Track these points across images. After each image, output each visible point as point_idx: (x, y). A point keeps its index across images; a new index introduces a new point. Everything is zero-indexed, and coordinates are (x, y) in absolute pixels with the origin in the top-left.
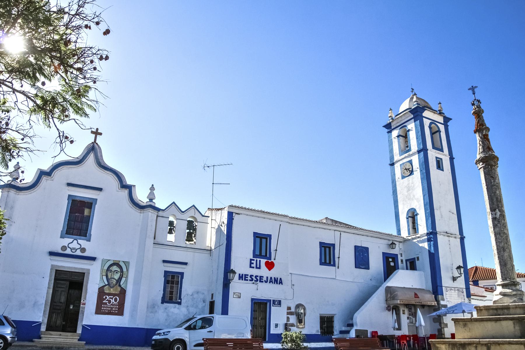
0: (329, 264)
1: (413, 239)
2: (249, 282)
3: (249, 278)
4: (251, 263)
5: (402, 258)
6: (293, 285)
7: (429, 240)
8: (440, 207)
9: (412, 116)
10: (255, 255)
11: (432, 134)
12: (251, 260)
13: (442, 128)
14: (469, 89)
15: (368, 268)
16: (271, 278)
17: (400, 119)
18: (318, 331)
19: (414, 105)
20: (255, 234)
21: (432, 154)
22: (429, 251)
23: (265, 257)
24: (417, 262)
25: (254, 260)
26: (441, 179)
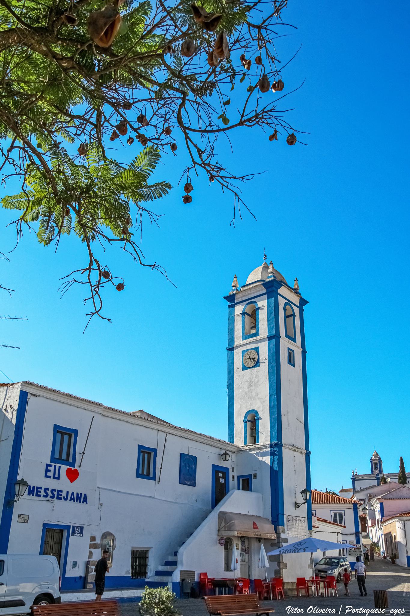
0: (147, 476)
1: (251, 450)
2: (42, 498)
3: (43, 493)
4: (47, 471)
6: (101, 505)
7: (272, 454)
8: (288, 413)
9: (265, 291)
10: (53, 459)
11: (287, 317)
12: (48, 465)
13: (297, 311)
15: (194, 485)
16: (73, 493)
17: (249, 292)
18: (128, 572)
19: (269, 277)
20: (56, 426)
21: (285, 344)
22: (272, 468)
23: (66, 462)
24: (253, 480)
25: (51, 466)
26: (290, 375)
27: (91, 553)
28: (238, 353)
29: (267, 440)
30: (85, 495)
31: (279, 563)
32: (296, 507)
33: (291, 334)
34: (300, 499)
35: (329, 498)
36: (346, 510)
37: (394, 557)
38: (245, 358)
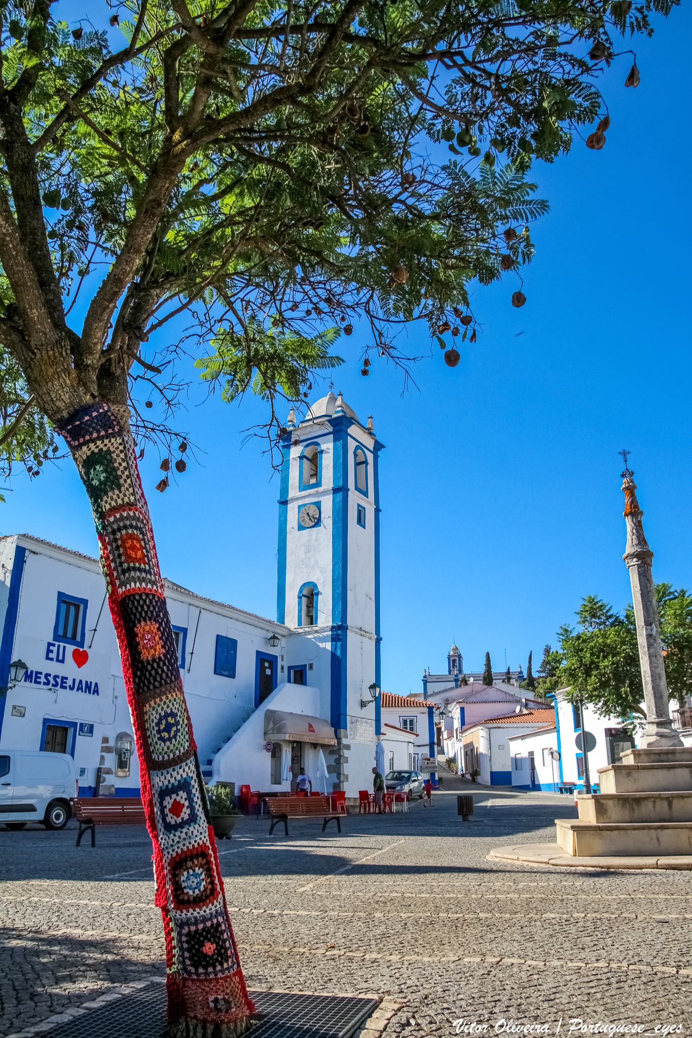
2: (42, 686)
3: (43, 680)
4: (49, 651)
5: (283, 663)
7: (334, 639)
9: (331, 429)
10: (56, 637)
11: (358, 464)
12: (49, 644)
13: (370, 457)
14: (620, 453)
15: (232, 675)
16: (81, 682)
17: (309, 429)
19: (337, 412)
20: (60, 594)
21: (354, 499)
22: (333, 655)
23: (72, 640)
25: (54, 645)
26: (360, 539)
27: (102, 758)
28: (293, 508)
29: (327, 622)
30: (96, 684)
31: (339, 775)
32: (362, 706)
33: (362, 486)
34: (368, 696)
35: (395, 702)
36: (419, 716)
37: (475, 774)
38: (302, 515)
